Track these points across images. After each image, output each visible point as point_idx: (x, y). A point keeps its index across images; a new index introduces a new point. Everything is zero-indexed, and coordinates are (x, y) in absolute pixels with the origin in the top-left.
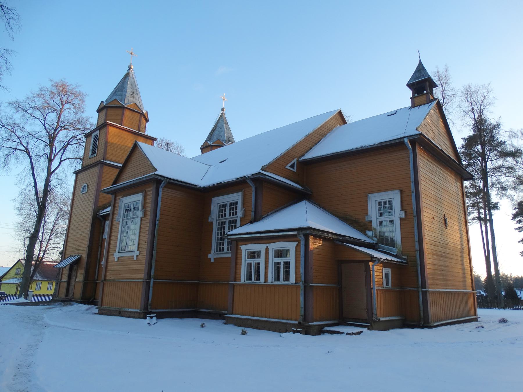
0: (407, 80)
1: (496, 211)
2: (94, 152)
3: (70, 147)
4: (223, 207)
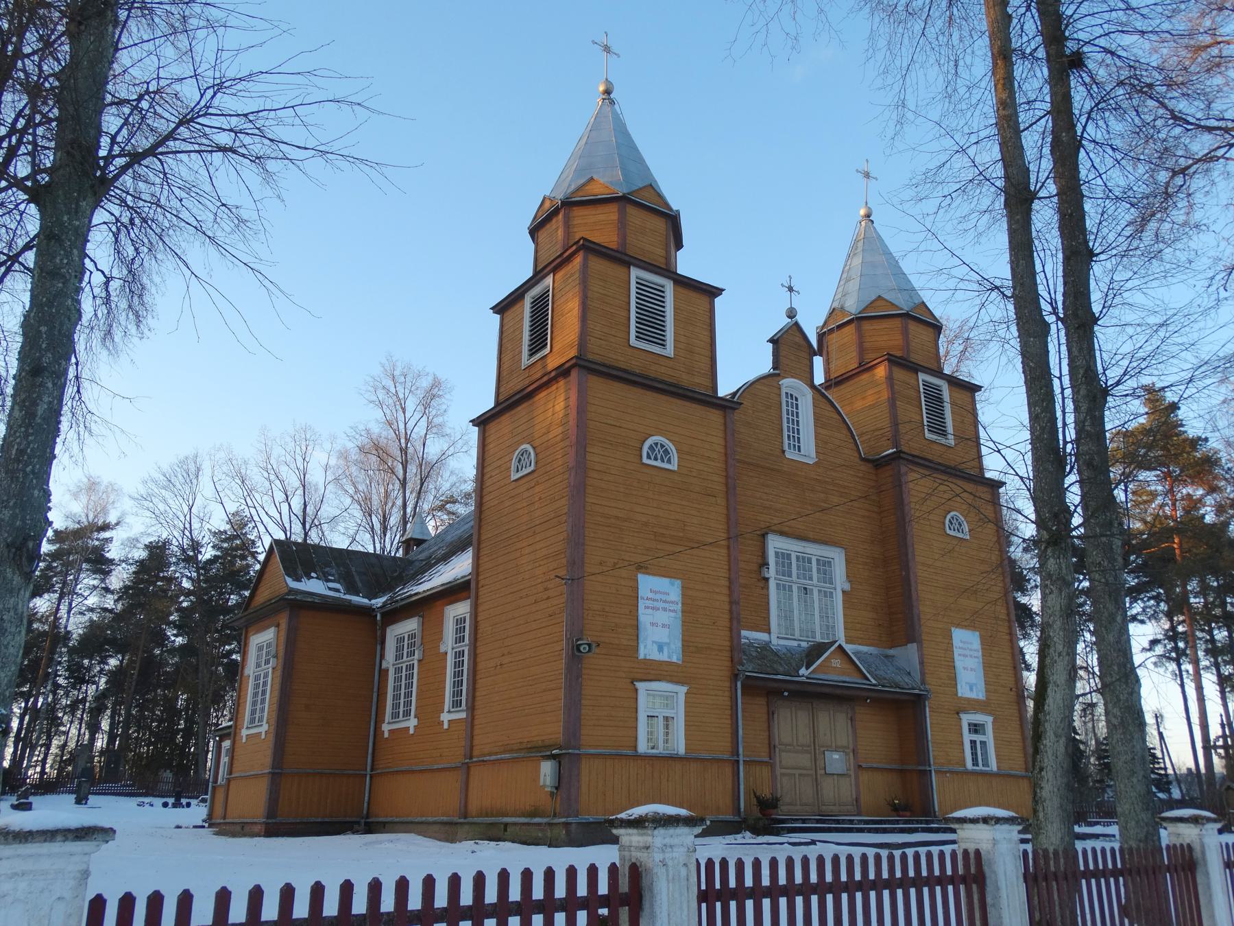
0: (772, 331)
1: (74, 801)
2: (538, 342)
3: (1071, 45)
4: (400, 640)
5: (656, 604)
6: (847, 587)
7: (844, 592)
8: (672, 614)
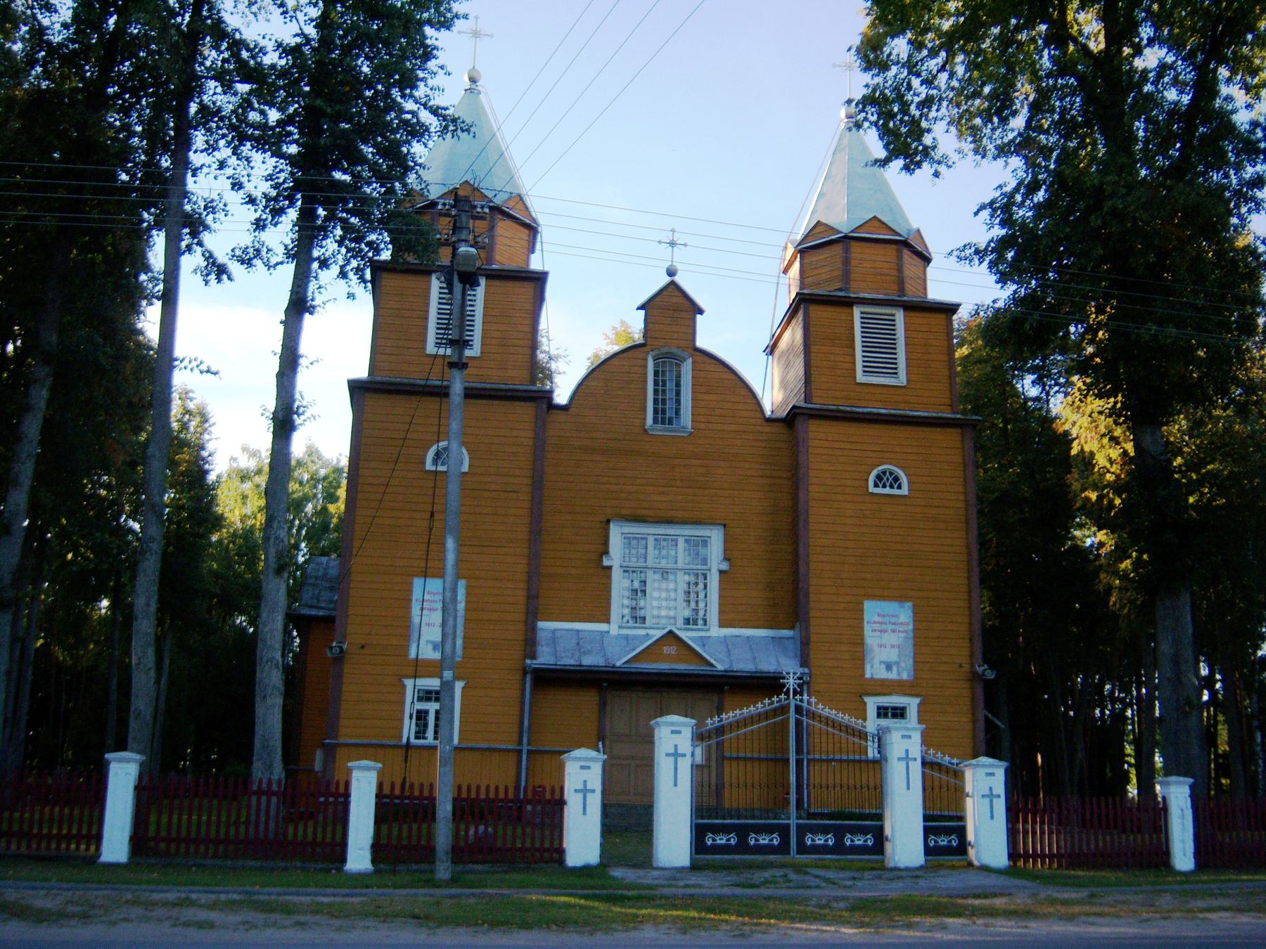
5: (884, 627)
6: (725, 566)
7: (721, 572)
8: (902, 635)
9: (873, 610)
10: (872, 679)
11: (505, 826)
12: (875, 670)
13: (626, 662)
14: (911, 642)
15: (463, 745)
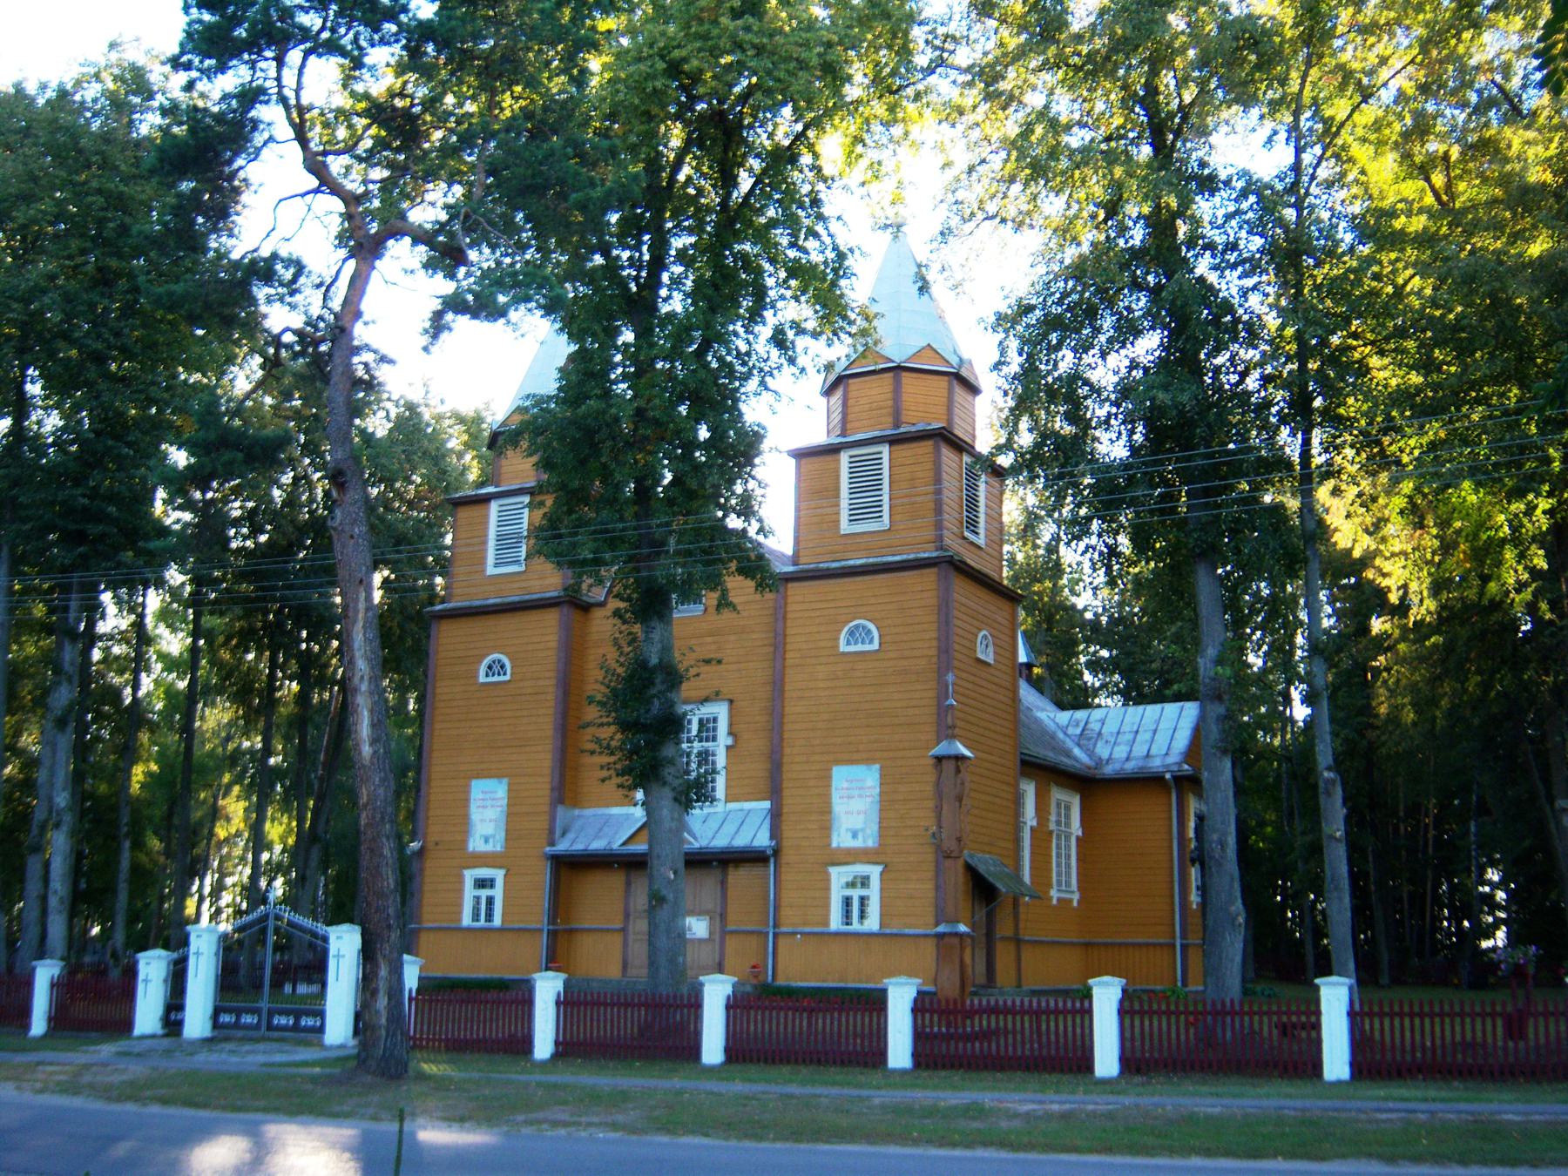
9: (479, 788)
10: (838, 849)
11: (997, 1028)
12: (841, 839)
13: (624, 844)
14: (877, 807)
15: (508, 925)
